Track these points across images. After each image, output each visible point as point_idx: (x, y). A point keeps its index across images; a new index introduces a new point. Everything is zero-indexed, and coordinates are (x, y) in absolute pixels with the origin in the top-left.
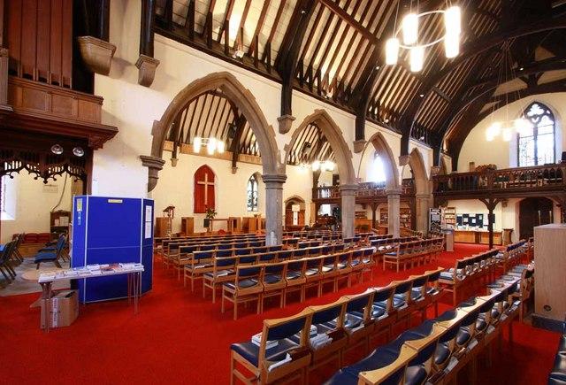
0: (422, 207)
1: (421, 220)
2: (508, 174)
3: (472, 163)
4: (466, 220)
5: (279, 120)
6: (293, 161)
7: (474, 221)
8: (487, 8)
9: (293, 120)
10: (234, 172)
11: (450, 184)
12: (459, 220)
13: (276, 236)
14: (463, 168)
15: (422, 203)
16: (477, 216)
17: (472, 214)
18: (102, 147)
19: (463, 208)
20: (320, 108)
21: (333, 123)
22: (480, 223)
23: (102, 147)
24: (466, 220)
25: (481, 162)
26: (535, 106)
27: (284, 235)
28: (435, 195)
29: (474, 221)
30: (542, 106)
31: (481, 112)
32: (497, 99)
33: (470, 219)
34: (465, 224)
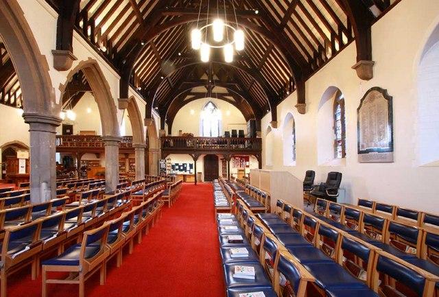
0: (154, 158)
1: (153, 168)
2: (201, 140)
3: (180, 131)
4: (177, 167)
5: (54, 53)
6: (12, 100)
7: (182, 168)
8: (260, 59)
9: (74, 59)
10: (302, 111)
11: (172, 142)
12: (173, 167)
13: (50, 187)
14: (175, 133)
15: (154, 155)
16: (184, 164)
17: (181, 164)
18: (356, 68)
19: (175, 159)
20: (93, 58)
21: (102, 74)
22: (185, 169)
23: (356, 68)
24: (177, 167)
25: (185, 131)
26: (210, 104)
27: (58, 185)
28: (162, 150)
29: (182, 168)
30: (214, 105)
31: (185, 99)
32: (193, 94)
33: (180, 166)
34: (177, 170)
